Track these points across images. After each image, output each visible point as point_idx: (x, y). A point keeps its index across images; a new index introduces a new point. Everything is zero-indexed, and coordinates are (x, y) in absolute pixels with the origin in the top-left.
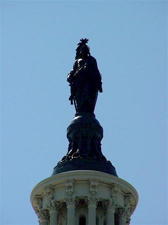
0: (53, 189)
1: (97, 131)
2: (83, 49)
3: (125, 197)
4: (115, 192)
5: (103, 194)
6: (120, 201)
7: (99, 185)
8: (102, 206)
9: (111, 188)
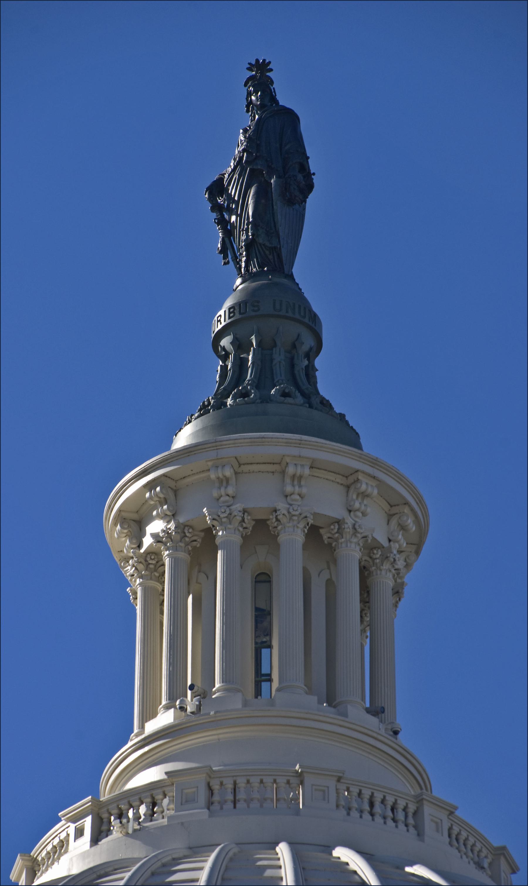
2: (260, 77)
3: (390, 516)
8: (319, 538)
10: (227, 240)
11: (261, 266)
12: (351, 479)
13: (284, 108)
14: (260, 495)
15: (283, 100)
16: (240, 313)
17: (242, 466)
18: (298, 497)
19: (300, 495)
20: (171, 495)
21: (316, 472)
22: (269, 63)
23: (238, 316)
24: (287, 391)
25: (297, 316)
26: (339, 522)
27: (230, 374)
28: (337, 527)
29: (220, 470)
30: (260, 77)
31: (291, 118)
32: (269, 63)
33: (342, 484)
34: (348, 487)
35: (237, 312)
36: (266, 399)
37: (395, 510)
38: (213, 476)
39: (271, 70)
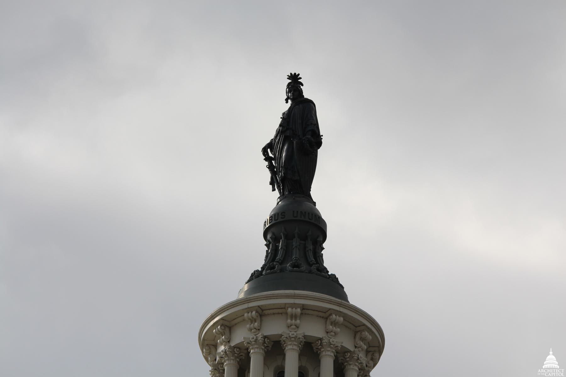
0: (261, 316)
1: (315, 140)
2: (295, 84)
3: (355, 333)
4: (334, 323)
5: (313, 329)
6: (345, 341)
7: (302, 314)
9: (355, 333)
10: (274, 177)
11: (289, 192)
12: (328, 314)
13: (307, 99)
14: (274, 328)
15: (307, 93)
16: (275, 220)
17: (264, 312)
18: (294, 327)
19: (296, 326)
20: (227, 330)
21: (307, 312)
22: (299, 74)
23: (273, 222)
24: (296, 264)
25: (307, 219)
26: (321, 339)
27: (269, 255)
28: (320, 342)
29: (294, 309)
30: (295, 84)
31: (309, 106)
32: (299, 74)
33: (323, 317)
34: (327, 318)
35: (273, 219)
36: (282, 270)
37: (358, 329)
38: (298, 321)
39: (300, 78)
